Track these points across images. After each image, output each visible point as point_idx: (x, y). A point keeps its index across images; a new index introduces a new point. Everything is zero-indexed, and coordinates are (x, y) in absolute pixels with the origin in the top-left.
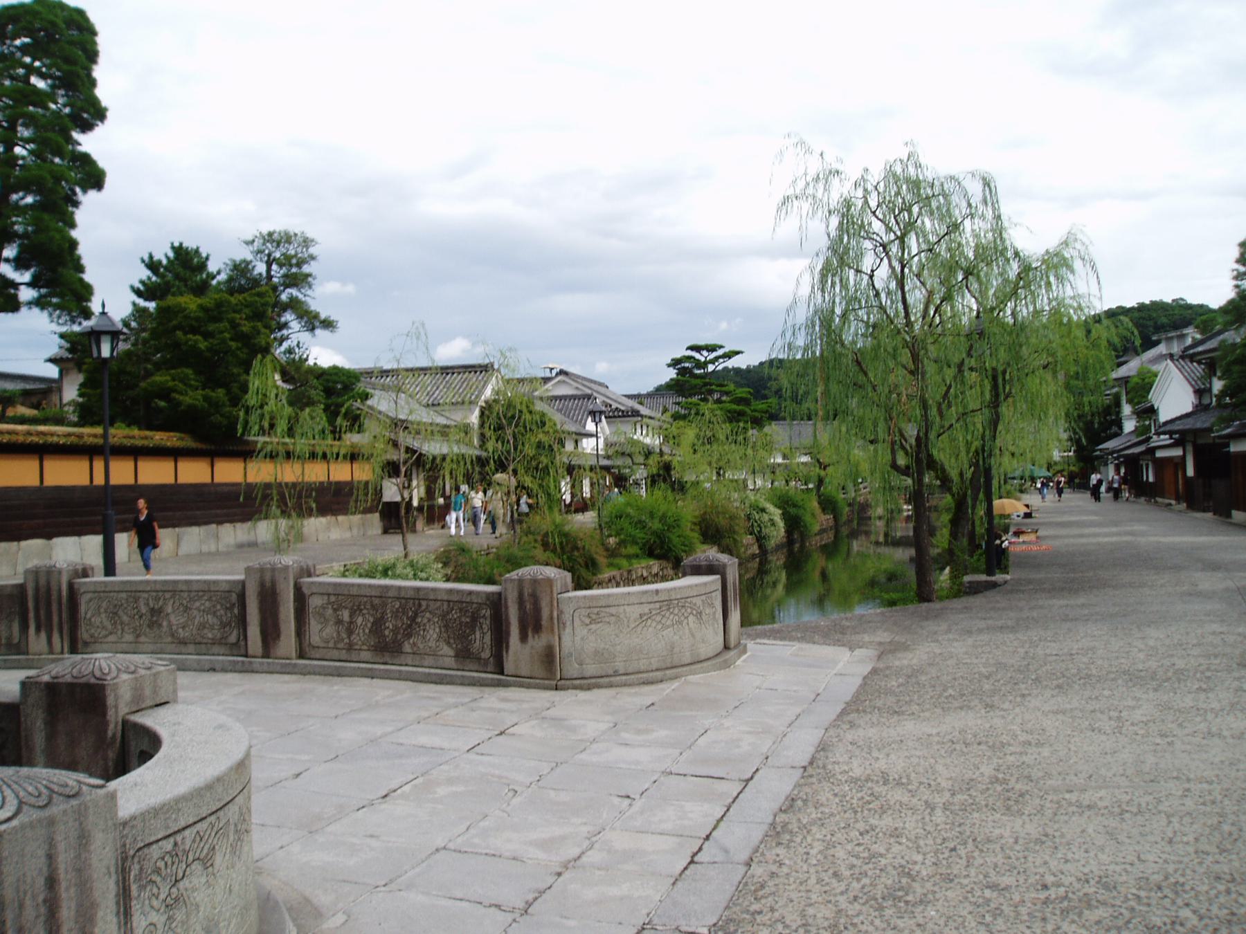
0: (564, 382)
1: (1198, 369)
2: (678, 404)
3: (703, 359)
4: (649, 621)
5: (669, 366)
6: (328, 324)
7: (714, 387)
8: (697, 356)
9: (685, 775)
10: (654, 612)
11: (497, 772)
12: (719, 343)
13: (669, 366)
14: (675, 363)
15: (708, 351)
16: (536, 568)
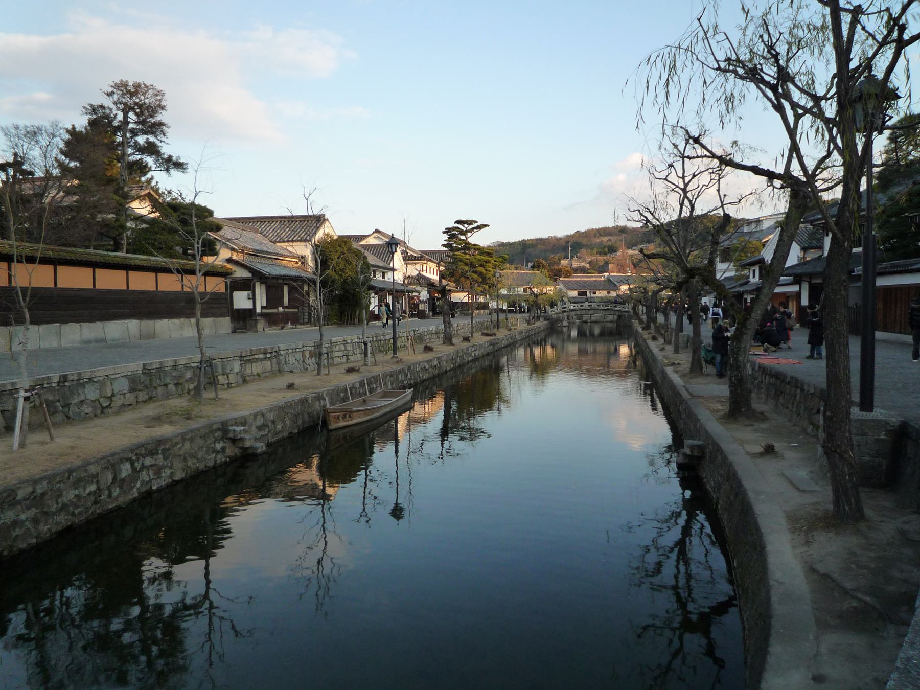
0: (378, 237)
3: (464, 229)
5: (444, 232)
6: (179, 166)
13: (444, 232)
14: (448, 231)
16: (399, 426)
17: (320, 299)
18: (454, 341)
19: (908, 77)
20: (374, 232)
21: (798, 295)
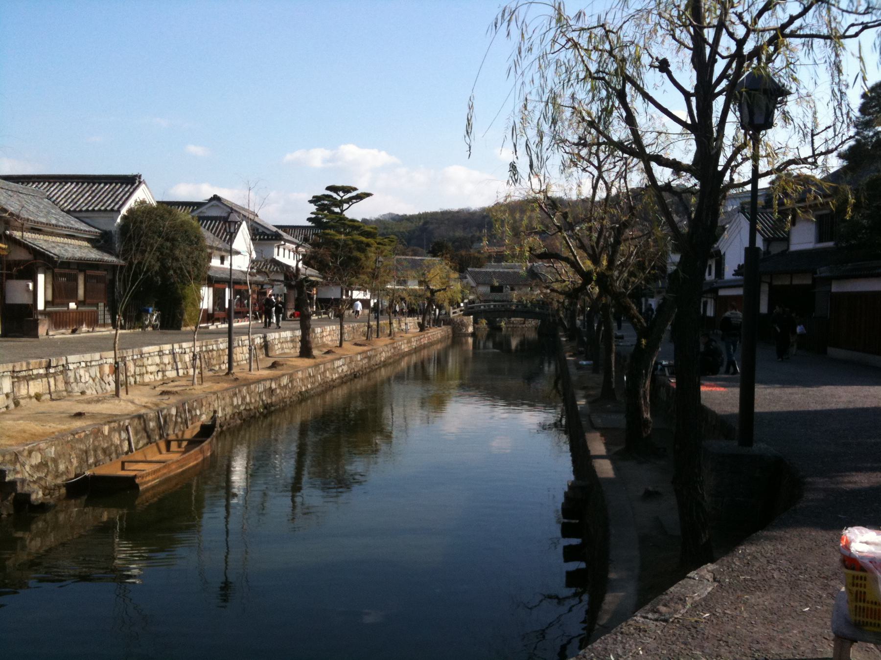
3: (339, 198)
5: (311, 202)
7: (346, 222)
8: (335, 195)
12: (353, 185)
13: (311, 202)
14: (316, 200)
18: (315, 352)
20: (211, 200)
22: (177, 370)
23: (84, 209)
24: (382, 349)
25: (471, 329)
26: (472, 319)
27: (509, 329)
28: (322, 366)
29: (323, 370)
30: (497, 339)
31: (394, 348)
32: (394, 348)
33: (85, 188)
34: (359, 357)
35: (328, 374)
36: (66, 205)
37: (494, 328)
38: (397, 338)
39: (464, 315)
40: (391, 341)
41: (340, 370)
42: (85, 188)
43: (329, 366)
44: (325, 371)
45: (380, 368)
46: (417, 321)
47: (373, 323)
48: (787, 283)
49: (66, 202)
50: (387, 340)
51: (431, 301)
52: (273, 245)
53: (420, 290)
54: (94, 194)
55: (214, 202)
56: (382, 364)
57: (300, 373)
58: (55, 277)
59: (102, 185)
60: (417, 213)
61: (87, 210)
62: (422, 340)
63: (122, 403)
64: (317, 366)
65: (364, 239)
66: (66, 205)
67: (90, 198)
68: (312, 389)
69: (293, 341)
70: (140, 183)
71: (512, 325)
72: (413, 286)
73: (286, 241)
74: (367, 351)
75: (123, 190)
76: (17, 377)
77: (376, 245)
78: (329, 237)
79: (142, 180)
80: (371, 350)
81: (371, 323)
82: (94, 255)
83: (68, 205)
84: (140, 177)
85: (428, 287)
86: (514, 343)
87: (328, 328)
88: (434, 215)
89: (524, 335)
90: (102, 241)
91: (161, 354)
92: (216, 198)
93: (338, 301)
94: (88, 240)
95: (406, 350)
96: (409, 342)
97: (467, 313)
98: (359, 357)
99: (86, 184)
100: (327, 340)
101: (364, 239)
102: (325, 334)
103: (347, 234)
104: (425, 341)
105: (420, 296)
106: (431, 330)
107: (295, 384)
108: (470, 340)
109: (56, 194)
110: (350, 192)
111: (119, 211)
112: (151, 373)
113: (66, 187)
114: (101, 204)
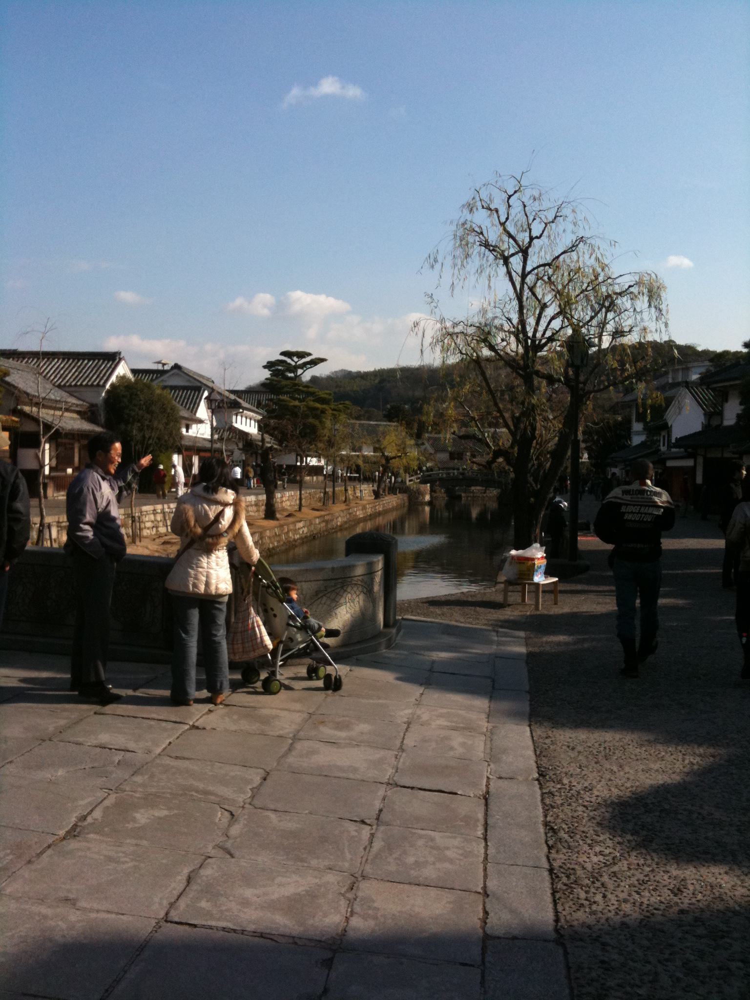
1: (710, 395)
2: (271, 400)
3: (293, 364)
4: (325, 598)
5: (265, 367)
7: (301, 388)
8: (289, 361)
9: (412, 788)
10: (329, 590)
11: (201, 786)
12: (308, 350)
13: (265, 367)
14: (270, 365)
15: (298, 357)
17: (211, 928)
18: (278, 516)
19: (621, 276)
21: (693, 469)
22: (167, 526)
23: (73, 384)
24: (339, 514)
25: (427, 498)
26: (429, 488)
27: (469, 498)
28: (286, 527)
29: (286, 530)
30: (457, 508)
31: (350, 514)
32: (350, 514)
33: (71, 364)
34: (317, 521)
35: (291, 534)
36: (56, 380)
37: (453, 498)
38: (353, 504)
39: (421, 483)
40: (347, 507)
41: (301, 532)
42: (71, 364)
43: (291, 527)
44: (288, 532)
45: (336, 532)
46: (372, 488)
47: (329, 490)
48: (719, 455)
49: (55, 377)
50: (343, 506)
51: (386, 469)
52: (231, 412)
53: (374, 456)
54: (80, 369)
55: (175, 371)
56: (338, 528)
57: (268, 531)
58: (58, 446)
59: (86, 361)
60: (372, 369)
61: (76, 385)
62: (377, 507)
63: (139, 548)
64: (281, 526)
65: (318, 405)
66: (56, 380)
67: (77, 373)
68: (278, 547)
69: (256, 505)
70: (120, 360)
71: (471, 495)
72: (368, 452)
73: (245, 409)
74: (325, 515)
75: (106, 366)
76: (61, 527)
77: (331, 412)
78: (284, 403)
79: (121, 357)
80: (328, 514)
81: (327, 490)
82: (86, 426)
83: (57, 381)
84: (120, 353)
85: (383, 455)
86: (475, 513)
87: (287, 494)
88: (391, 372)
89: (485, 505)
90: (89, 414)
91: (155, 512)
92: (177, 367)
93: (292, 468)
94: (78, 413)
95: (361, 516)
96: (364, 508)
97: (424, 481)
98: (317, 521)
99: (71, 361)
100: (287, 504)
101: (318, 405)
102: (284, 499)
103: (300, 400)
104: (380, 508)
105: (375, 463)
106: (386, 498)
107: (264, 541)
108: (427, 509)
109: (45, 369)
110: (305, 357)
111: (104, 386)
112: (148, 528)
113: (53, 363)
114: (88, 379)
